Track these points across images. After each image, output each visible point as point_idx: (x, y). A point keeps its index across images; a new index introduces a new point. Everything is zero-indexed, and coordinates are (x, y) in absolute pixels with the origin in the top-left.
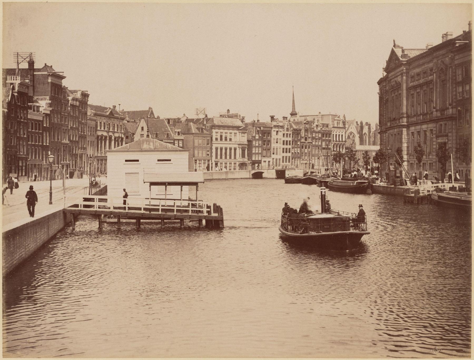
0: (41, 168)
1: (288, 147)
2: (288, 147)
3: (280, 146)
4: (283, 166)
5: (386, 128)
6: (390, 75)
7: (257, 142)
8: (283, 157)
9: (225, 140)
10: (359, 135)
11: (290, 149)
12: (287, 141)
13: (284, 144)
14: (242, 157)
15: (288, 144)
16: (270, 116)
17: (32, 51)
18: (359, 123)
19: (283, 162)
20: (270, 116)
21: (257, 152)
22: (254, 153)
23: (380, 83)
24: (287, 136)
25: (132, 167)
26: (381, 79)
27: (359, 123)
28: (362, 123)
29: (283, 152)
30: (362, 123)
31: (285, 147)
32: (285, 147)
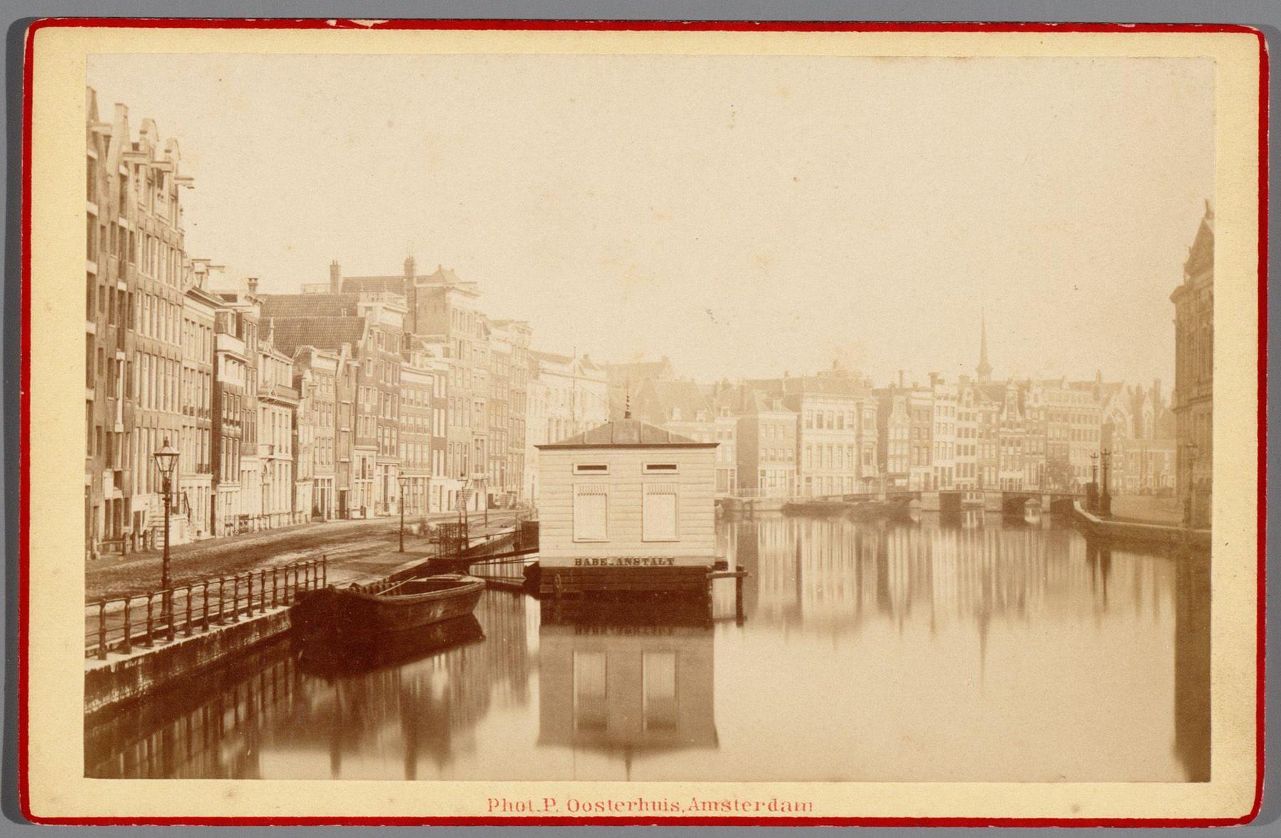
0: (428, 486)
1: (971, 441)
2: (971, 441)
3: (951, 438)
4: (958, 486)
5: (1190, 400)
6: (1198, 281)
7: (899, 431)
8: (958, 465)
9: (807, 427)
10: (1131, 417)
11: (973, 447)
12: (966, 447)
13: (959, 436)
14: (93, 672)
15: (970, 435)
16: (929, 374)
17: (138, 132)
18: (1133, 390)
19: (958, 475)
20: (929, 374)
21: (898, 452)
22: (892, 456)
23: (1175, 298)
24: (966, 447)
25: (661, 478)
26: (1180, 288)
27: (1133, 390)
28: (1139, 388)
29: (959, 454)
30: (1139, 388)
31: (963, 441)
32: (963, 441)
